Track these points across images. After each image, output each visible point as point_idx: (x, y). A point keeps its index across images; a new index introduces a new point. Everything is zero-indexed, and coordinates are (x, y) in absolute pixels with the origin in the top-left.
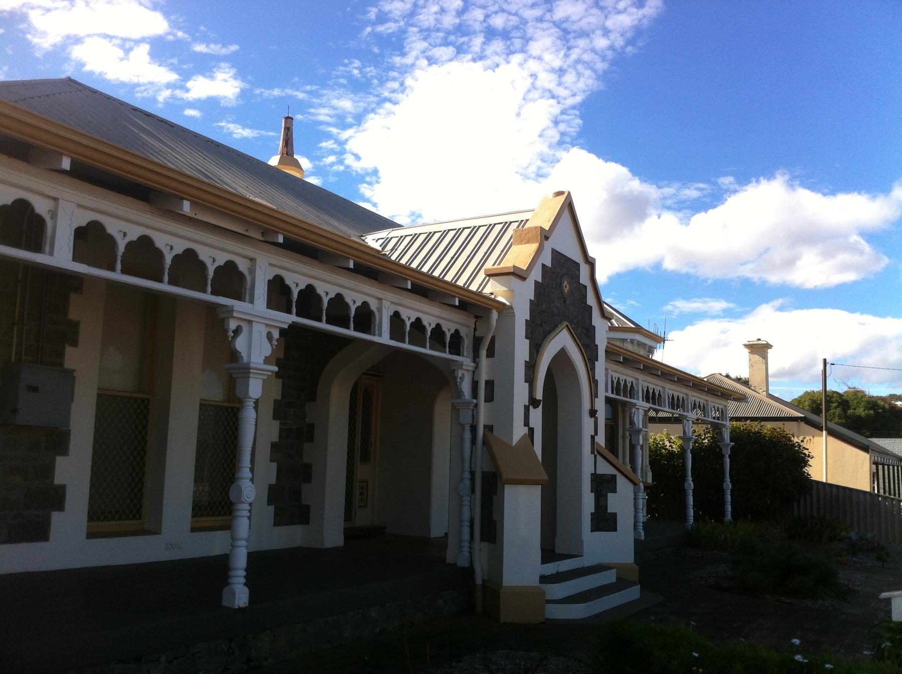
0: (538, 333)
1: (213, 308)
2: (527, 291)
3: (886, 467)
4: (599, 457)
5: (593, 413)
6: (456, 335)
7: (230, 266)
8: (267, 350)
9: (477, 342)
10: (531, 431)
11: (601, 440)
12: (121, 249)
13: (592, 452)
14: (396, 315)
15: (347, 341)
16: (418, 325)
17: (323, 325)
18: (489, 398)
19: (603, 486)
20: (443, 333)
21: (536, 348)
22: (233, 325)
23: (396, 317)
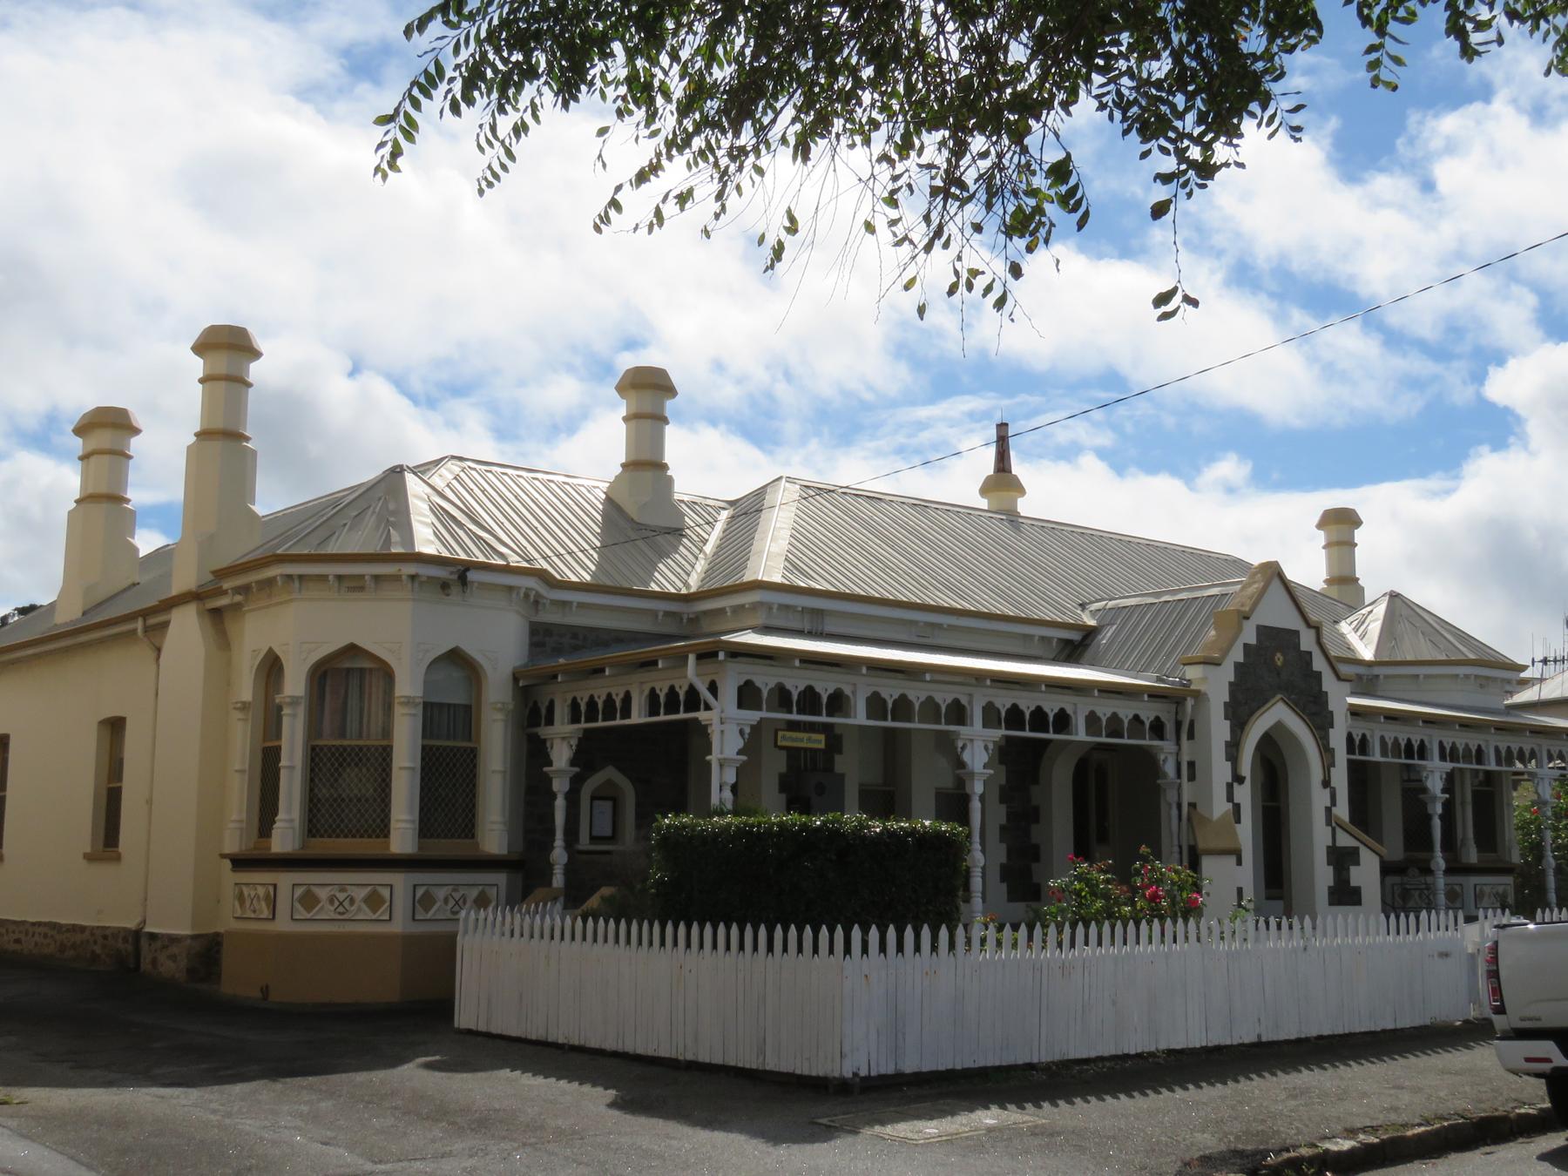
2: (1227, 674)
3: (494, 831)
4: (1338, 830)
5: (1326, 783)
6: (1479, 750)
7: (956, 702)
8: (985, 758)
9: (1178, 725)
10: (1237, 807)
11: (1342, 811)
12: (795, 698)
13: (1328, 823)
14: (1441, 743)
15: (1050, 741)
17: (1027, 734)
18: (1192, 778)
19: (1342, 859)
22: (960, 744)
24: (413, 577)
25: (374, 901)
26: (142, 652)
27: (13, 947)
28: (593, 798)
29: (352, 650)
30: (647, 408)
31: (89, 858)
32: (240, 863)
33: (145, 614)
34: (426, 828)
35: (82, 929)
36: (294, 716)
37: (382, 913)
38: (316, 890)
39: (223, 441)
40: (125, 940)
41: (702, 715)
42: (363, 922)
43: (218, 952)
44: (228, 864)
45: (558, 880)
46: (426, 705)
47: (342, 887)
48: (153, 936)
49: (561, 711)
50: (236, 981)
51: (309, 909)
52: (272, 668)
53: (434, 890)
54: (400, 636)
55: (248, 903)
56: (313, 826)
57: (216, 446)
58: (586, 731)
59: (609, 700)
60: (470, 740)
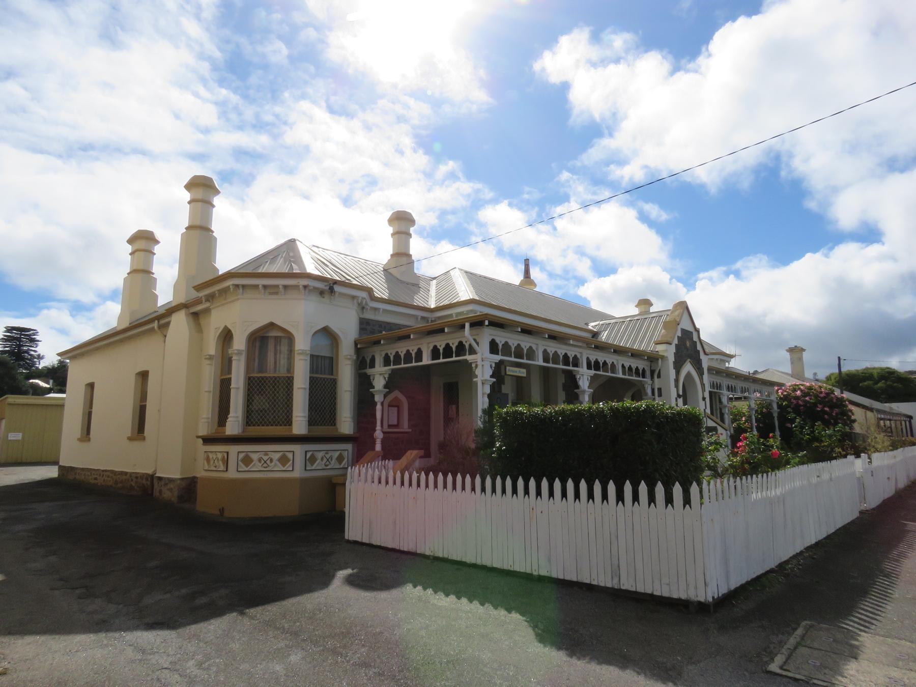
0: (678, 366)
1: (570, 372)
3: (346, 424)
5: (704, 399)
6: (644, 370)
9: (652, 372)
14: (588, 359)
16: (630, 368)
20: (497, 345)
21: (678, 373)
23: (623, 366)
24: (305, 287)
25: (283, 460)
26: (157, 338)
27: (93, 481)
28: (389, 406)
29: (272, 325)
30: (403, 229)
31: (130, 439)
32: (208, 440)
33: (159, 318)
34: (311, 422)
35: (126, 473)
36: (239, 360)
37: (288, 467)
38: (250, 454)
39: (200, 234)
40: (147, 479)
41: (469, 358)
42: (278, 472)
43: (195, 486)
44: (201, 441)
45: (378, 447)
46: (312, 356)
47: (266, 453)
48: (160, 478)
49: (379, 361)
50: (205, 505)
51: (247, 466)
52: (227, 336)
53: (315, 453)
54: (300, 318)
55: (212, 462)
56: (249, 419)
57: (197, 233)
58: (393, 370)
59: (408, 353)
60: (332, 374)
